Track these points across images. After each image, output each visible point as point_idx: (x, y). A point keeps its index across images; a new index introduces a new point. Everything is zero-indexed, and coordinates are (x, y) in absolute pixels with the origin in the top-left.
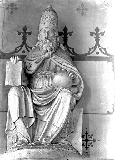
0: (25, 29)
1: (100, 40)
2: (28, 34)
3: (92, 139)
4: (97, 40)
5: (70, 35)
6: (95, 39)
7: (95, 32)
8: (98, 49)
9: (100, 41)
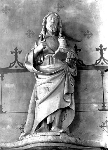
0: (16, 49)
1: (18, 57)
2: (78, 51)
3: (22, 129)
4: (102, 54)
5: (20, 53)
6: (100, 53)
7: (100, 48)
8: (102, 61)
9: (18, 58)
